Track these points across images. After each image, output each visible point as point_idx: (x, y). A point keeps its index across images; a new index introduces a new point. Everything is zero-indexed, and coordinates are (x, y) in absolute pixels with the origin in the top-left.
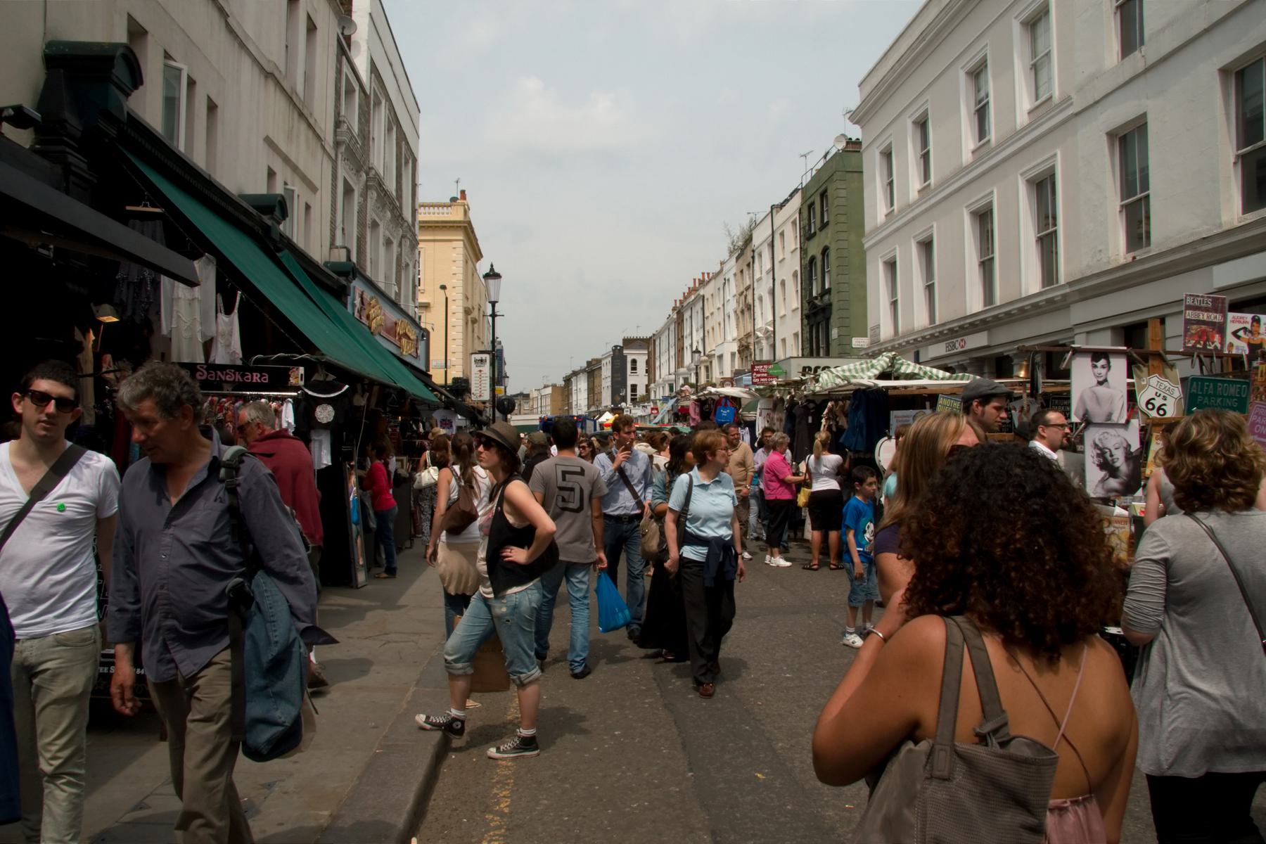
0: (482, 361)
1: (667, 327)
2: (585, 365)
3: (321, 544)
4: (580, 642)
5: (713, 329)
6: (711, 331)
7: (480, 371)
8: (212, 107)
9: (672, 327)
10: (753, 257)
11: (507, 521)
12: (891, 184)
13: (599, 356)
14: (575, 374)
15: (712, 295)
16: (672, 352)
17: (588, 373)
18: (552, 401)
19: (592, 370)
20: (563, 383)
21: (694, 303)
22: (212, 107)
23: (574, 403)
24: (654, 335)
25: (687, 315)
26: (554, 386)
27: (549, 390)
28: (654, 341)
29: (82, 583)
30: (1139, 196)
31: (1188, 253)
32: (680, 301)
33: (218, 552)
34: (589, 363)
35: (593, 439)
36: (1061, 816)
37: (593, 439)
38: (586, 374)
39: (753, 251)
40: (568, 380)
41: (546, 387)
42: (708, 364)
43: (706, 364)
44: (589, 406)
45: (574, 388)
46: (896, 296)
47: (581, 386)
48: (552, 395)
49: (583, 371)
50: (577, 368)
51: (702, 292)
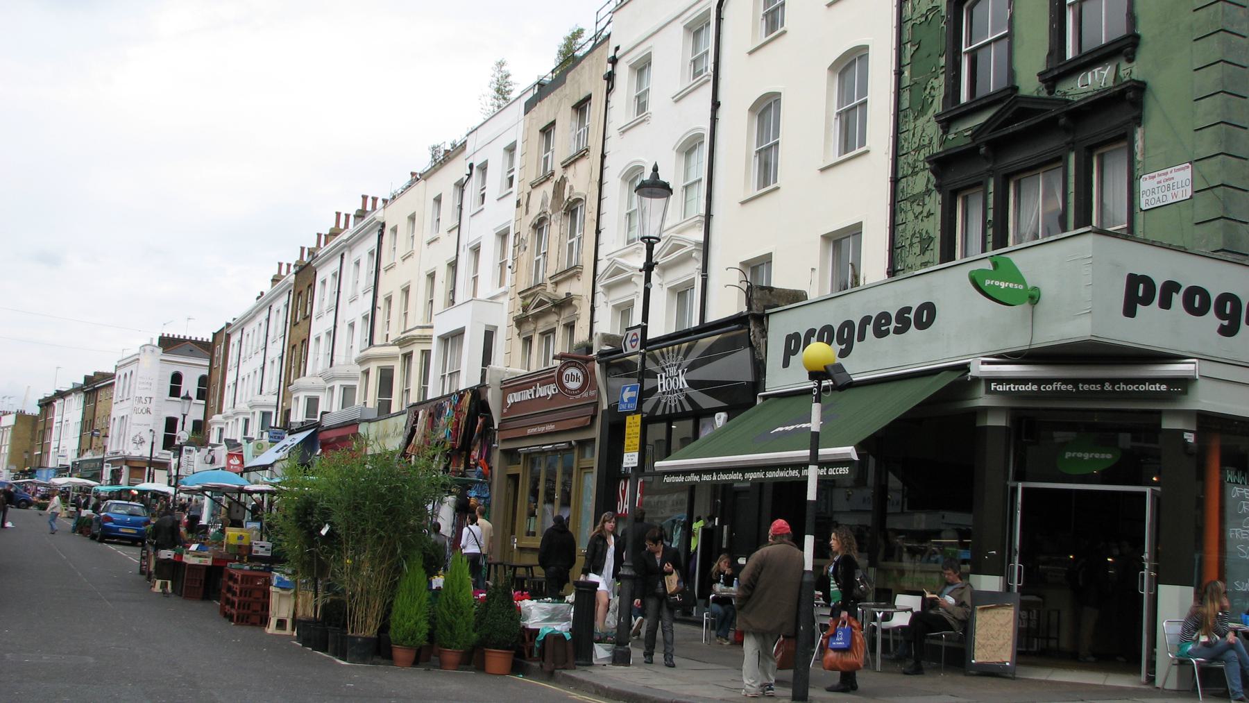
1: (265, 303)
2: (82, 381)
4: (1209, 604)
5: (406, 291)
6: (122, 377)
9: (280, 304)
10: (610, 77)
13: (110, 369)
14: (61, 395)
15: (412, 218)
16: (275, 350)
17: (86, 393)
23: (54, 444)
24: (228, 325)
25: (325, 273)
26: (20, 416)
28: (228, 336)
30: (771, 142)
32: (325, 235)
34: (88, 379)
35: (509, 401)
37: (509, 401)
38: (82, 395)
39: (614, 61)
40: (47, 404)
42: (223, 426)
43: (246, 417)
44: (81, 452)
45: (57, 418)
46: (390, 395)
48: (14, 428)
49: (76, 390)
50: (66, 386)
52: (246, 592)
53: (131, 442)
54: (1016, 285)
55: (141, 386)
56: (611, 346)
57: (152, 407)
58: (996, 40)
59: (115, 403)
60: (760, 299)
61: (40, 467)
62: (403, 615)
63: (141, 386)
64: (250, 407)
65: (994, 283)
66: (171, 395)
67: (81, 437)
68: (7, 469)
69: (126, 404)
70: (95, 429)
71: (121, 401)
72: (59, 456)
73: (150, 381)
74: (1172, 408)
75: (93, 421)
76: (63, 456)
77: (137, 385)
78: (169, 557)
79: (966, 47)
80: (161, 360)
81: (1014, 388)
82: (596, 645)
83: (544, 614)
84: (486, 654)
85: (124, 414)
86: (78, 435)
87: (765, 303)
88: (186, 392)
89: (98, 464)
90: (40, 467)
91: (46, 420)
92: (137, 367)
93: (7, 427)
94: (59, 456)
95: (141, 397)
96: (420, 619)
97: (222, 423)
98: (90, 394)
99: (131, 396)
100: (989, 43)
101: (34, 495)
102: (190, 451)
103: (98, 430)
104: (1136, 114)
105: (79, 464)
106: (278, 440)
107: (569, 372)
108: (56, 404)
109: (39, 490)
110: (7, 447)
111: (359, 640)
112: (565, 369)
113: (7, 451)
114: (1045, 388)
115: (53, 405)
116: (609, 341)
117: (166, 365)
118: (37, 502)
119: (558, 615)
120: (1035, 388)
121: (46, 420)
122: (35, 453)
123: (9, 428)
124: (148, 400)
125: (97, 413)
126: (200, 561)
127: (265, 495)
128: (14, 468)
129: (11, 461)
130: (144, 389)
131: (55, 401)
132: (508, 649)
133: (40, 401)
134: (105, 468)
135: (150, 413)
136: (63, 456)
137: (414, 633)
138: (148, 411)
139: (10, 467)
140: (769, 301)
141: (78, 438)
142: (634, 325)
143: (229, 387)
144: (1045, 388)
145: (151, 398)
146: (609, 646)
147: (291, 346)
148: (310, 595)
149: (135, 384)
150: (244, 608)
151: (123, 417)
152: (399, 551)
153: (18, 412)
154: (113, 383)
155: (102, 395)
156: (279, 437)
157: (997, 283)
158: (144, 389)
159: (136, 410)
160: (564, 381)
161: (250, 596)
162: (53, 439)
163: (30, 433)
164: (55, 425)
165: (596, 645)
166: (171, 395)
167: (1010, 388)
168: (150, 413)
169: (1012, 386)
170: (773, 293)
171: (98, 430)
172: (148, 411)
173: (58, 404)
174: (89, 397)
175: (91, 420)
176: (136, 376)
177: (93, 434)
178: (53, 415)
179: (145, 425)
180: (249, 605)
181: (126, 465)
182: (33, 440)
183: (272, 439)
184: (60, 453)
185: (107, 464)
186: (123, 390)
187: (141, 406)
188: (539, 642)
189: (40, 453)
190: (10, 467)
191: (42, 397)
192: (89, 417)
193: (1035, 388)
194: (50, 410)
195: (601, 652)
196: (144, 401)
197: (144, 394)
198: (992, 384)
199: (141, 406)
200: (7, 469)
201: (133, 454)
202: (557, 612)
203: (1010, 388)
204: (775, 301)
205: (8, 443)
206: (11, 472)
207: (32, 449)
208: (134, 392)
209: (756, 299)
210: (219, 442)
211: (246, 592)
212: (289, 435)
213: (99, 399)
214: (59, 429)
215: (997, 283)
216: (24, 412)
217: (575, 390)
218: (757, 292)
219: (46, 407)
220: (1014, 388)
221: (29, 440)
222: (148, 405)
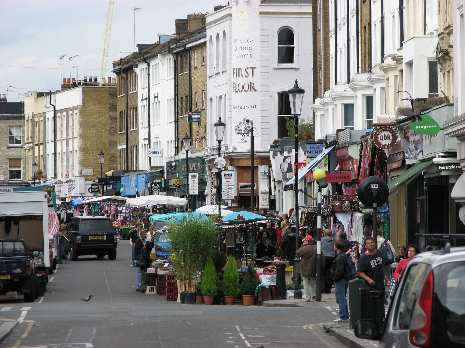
23: (143, 133)
45: (142, 93)
48: (83, 108)
52: (171, 277)
53: (234, 133)
54: (432, 126)
55: (239, 53)
56: (406, 116)
57: (257, 80)
59: (210, 77)
60: (418, 107)
61: (127, 171)
62: (205, 284)
63: (239, 53)
64: (323, 105)
65: (420, 127)
66: (281, 61)
67: (176, 122)
68: (81, 175)
69: (223, 78)
70: (193, 110)
71: (216, 74)
72: (152, 153)
73: (249, 45)
75: (189, 97)
76: (156, 152)
77: (234, 52)
78: (153, 272)
80: (261, 13)
81: (447, 168)
82: (288, 291)
83: (267, 279)
84: (243, 297)
85: (223, 94)
86: (173, 119)
87: (421, 108)
88: (218, 119)
89: (199, 164)
90: (127, 171)
91: (127, 96)
92: (231, 25)
93: (73, 109)
94: (152, 153)
95: (240, 69)
96: (212, 285)
97: (370, 88)
98: (181, 56)
99: (227, 68)
101: (115, 217)
102: (229, 175)
103: (197, 113)
105: (176, 165)
106: (316, 154)
107: (382, 134)
108: (137, 70)
109: (121, 212)
110: (76, 141)
111: (188, 294)
112: (379, 132)
113: (77, 147)
114: (457, 167)
115: (134, 72)
116: (404, 112)
118: (118, 228)
119: (274, 279)
120: (454, 167)
121: (127, 96)
122: (119, 148)
123: (76, 111)
124: (250, 71)
125: (194, 86)
126: (165, 273)
128: (91, 172)
129: (84, 164)
130: (242, 56)
131: (137, 66)
132: (250, 294)
133: (115, 64)
134: (191, 180)
135: (255, 90)
136: (156, 152)
137: (210, 290)
138: (251, 87)
139: (85, 172)
140: (424, 106)
141: (173, 124)
142: (411, 107)
143: (375, 25)
144: (457, 167)
145: (253, 69)
146: (294, 291)
147: (363, 27)
149: (230, 50)
150: (170, 292)
151: (221, 97)
152: (200, 258)
153: (85, 80)
154: (205, 43)
155: (196, 56)
156: (316, 152)
157: (422, 127)
158: (242, 56)
159: (235, 88)
160: (391, 137)
161: (173, 286)
162: (140, 126)
163: (107, 115)
164: (140, 103)
165: (288, 291)
166: (281, 61)
167: (445, 168)
168: (255, 90)
169: (446, 167)
170: (426, 102)
171: (197, 113)
172: (251, 87)
174: (181, 62)
175: (187, 97)
176: (231, 37)
177: (190, 118)
178: (136, 88)
179: (250, 107)
180: (173, 290)
181: (231, 165)
182: (113, 125)
183: (309, 154)
184: (153, 148)
185: (193, 174)
186: (218, 58)
187: (242, 81)
188: (257, 290)
189: (125, 146)
190: (85, 172)
191: (117, 59)
192: (183, 92)
193: (454, 167)
194: (131, 78)
195: (290, 293)
196: (244, 74)
197: (243, 64)
198: (440, 166)
199: (242, 81)
200: (81, 175)
201: (239, 150)
202: (273, 278)
203: (445, 168)
204: (428, 106)
205: (76, 134)
206: (86, 179)
207: (114, 141)
208: (231, 63)
209: (415, 107)
210: (346, 124)
211: (171, 277)
212: (326, 148)
213: (193, 64)
214: (147, 109)
215: (422, 127)
216: (96, 80)
217: (387, 146)
218: (415, 103)
219: (124, 75)
220: (447, 168)
221: (108, 127)
222: (250, 79)
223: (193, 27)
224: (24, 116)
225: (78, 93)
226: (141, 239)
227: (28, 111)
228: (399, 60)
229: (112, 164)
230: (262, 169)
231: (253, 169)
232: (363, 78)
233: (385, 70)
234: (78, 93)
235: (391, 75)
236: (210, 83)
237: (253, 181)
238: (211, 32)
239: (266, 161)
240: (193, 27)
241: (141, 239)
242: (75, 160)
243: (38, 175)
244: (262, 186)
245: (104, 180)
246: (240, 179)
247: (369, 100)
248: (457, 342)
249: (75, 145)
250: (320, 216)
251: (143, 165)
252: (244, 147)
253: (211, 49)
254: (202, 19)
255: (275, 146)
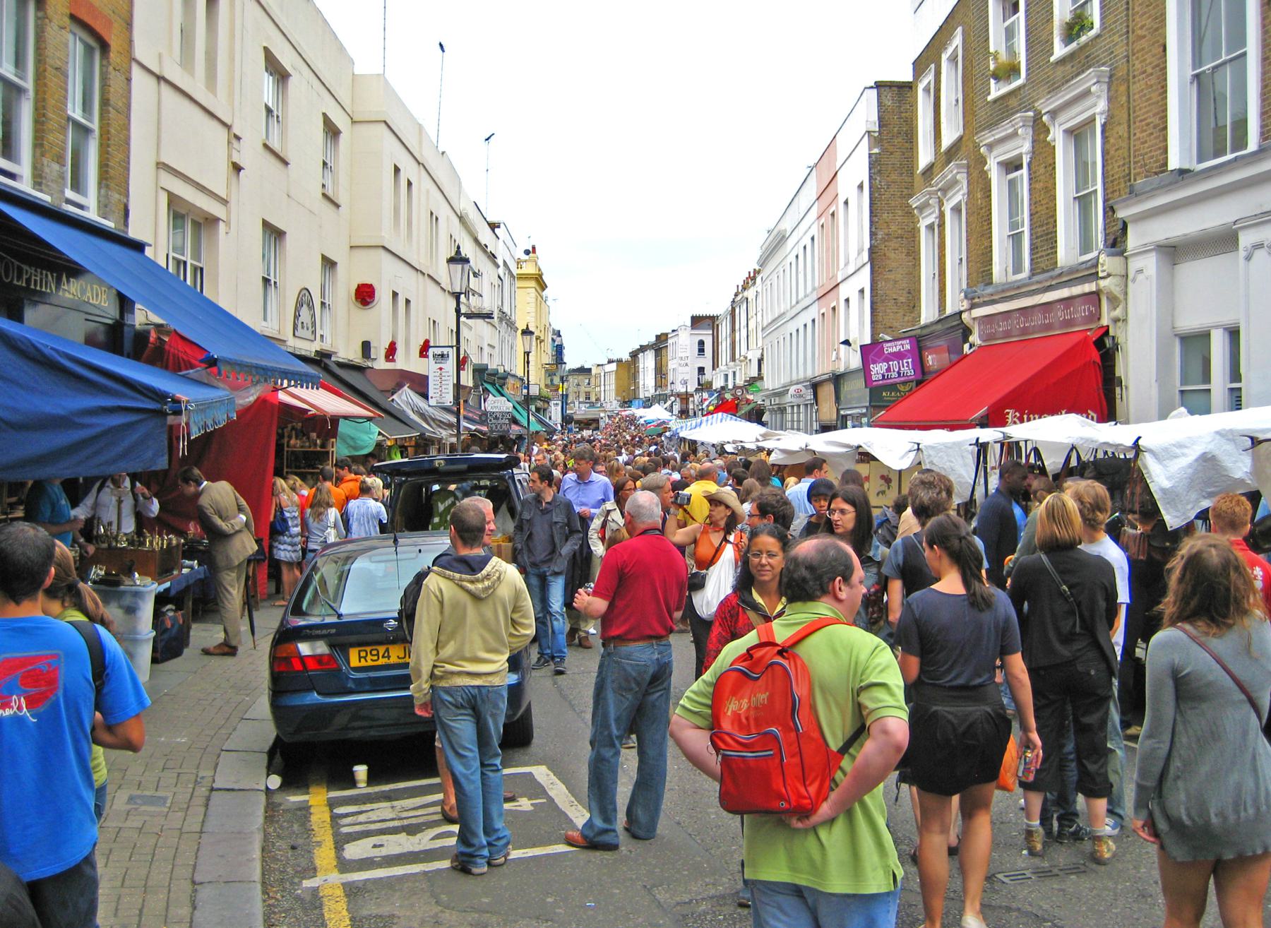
0: (442, 356)
2: (653, 339)
3: (1080, 668)
7: (441, 369)
8: (437, 219)
11: (1003, 750)
12: (528, 363)
14: (643, 349)
18: (617, 379)
19: (660, 345)
20: (630, 359)
21: (741, 301)
22: (437, 219)
23: (641, 383)
26: (619, 361)
27: (613, 367)
29: (487, 636)
30: (1091, 190)
31: (448, 572)
33: (831, 699)
34: (658, 337)
36: (900, 94)
40: (634, 355)
41: (610, 362)
45: (641, 366)
47: (648, 362)
51: (746, 294)
57: (688, 361)
58: (1231, 60)
69: (675, 361)
74: (1017, 627)
79: (1022, 175)
100: (1224, 63)
104: (503, 555)
117: (693, 337)
127: (1121, 214)
129: (617, 395)
148: (768, 907)
155: (664, 351)
159: (680, 365)
173: (641, 355)
187: (683, 362)
192: (658, 366)
197: (683, 355)
199: (683, 362)
207: (629, 385)
223: (663, 338)
224: (159, 327)
225: (615, 364)
226: (48, 582)
227: (594, 372)
228: (746, 358)
229: (629, 394)
230: (691, 399)
231: (687, 399)
232: (732, 363)
233: (741, 361)
234: (615, 364)
235: (743, 364)
236: (670, 363)
237: (687, 403)
238: (670, 341)
239: (692, 396)
240: (663, 338)
241: (48, 582)
242: (613, 394)
243: (598, 399)
244: (691, 406)
245: (625, 402)
246: (681, 403)
247: (734, 373)
248: (739, 570)
249: (613, 387)
250: (194, 626)
251: (641, 396)
252: (683, 390)
253: (670, 349)
254: (666, 335)
255: (697, 390)
